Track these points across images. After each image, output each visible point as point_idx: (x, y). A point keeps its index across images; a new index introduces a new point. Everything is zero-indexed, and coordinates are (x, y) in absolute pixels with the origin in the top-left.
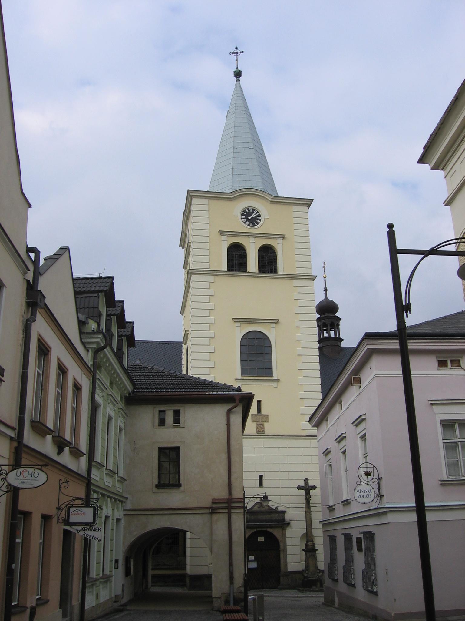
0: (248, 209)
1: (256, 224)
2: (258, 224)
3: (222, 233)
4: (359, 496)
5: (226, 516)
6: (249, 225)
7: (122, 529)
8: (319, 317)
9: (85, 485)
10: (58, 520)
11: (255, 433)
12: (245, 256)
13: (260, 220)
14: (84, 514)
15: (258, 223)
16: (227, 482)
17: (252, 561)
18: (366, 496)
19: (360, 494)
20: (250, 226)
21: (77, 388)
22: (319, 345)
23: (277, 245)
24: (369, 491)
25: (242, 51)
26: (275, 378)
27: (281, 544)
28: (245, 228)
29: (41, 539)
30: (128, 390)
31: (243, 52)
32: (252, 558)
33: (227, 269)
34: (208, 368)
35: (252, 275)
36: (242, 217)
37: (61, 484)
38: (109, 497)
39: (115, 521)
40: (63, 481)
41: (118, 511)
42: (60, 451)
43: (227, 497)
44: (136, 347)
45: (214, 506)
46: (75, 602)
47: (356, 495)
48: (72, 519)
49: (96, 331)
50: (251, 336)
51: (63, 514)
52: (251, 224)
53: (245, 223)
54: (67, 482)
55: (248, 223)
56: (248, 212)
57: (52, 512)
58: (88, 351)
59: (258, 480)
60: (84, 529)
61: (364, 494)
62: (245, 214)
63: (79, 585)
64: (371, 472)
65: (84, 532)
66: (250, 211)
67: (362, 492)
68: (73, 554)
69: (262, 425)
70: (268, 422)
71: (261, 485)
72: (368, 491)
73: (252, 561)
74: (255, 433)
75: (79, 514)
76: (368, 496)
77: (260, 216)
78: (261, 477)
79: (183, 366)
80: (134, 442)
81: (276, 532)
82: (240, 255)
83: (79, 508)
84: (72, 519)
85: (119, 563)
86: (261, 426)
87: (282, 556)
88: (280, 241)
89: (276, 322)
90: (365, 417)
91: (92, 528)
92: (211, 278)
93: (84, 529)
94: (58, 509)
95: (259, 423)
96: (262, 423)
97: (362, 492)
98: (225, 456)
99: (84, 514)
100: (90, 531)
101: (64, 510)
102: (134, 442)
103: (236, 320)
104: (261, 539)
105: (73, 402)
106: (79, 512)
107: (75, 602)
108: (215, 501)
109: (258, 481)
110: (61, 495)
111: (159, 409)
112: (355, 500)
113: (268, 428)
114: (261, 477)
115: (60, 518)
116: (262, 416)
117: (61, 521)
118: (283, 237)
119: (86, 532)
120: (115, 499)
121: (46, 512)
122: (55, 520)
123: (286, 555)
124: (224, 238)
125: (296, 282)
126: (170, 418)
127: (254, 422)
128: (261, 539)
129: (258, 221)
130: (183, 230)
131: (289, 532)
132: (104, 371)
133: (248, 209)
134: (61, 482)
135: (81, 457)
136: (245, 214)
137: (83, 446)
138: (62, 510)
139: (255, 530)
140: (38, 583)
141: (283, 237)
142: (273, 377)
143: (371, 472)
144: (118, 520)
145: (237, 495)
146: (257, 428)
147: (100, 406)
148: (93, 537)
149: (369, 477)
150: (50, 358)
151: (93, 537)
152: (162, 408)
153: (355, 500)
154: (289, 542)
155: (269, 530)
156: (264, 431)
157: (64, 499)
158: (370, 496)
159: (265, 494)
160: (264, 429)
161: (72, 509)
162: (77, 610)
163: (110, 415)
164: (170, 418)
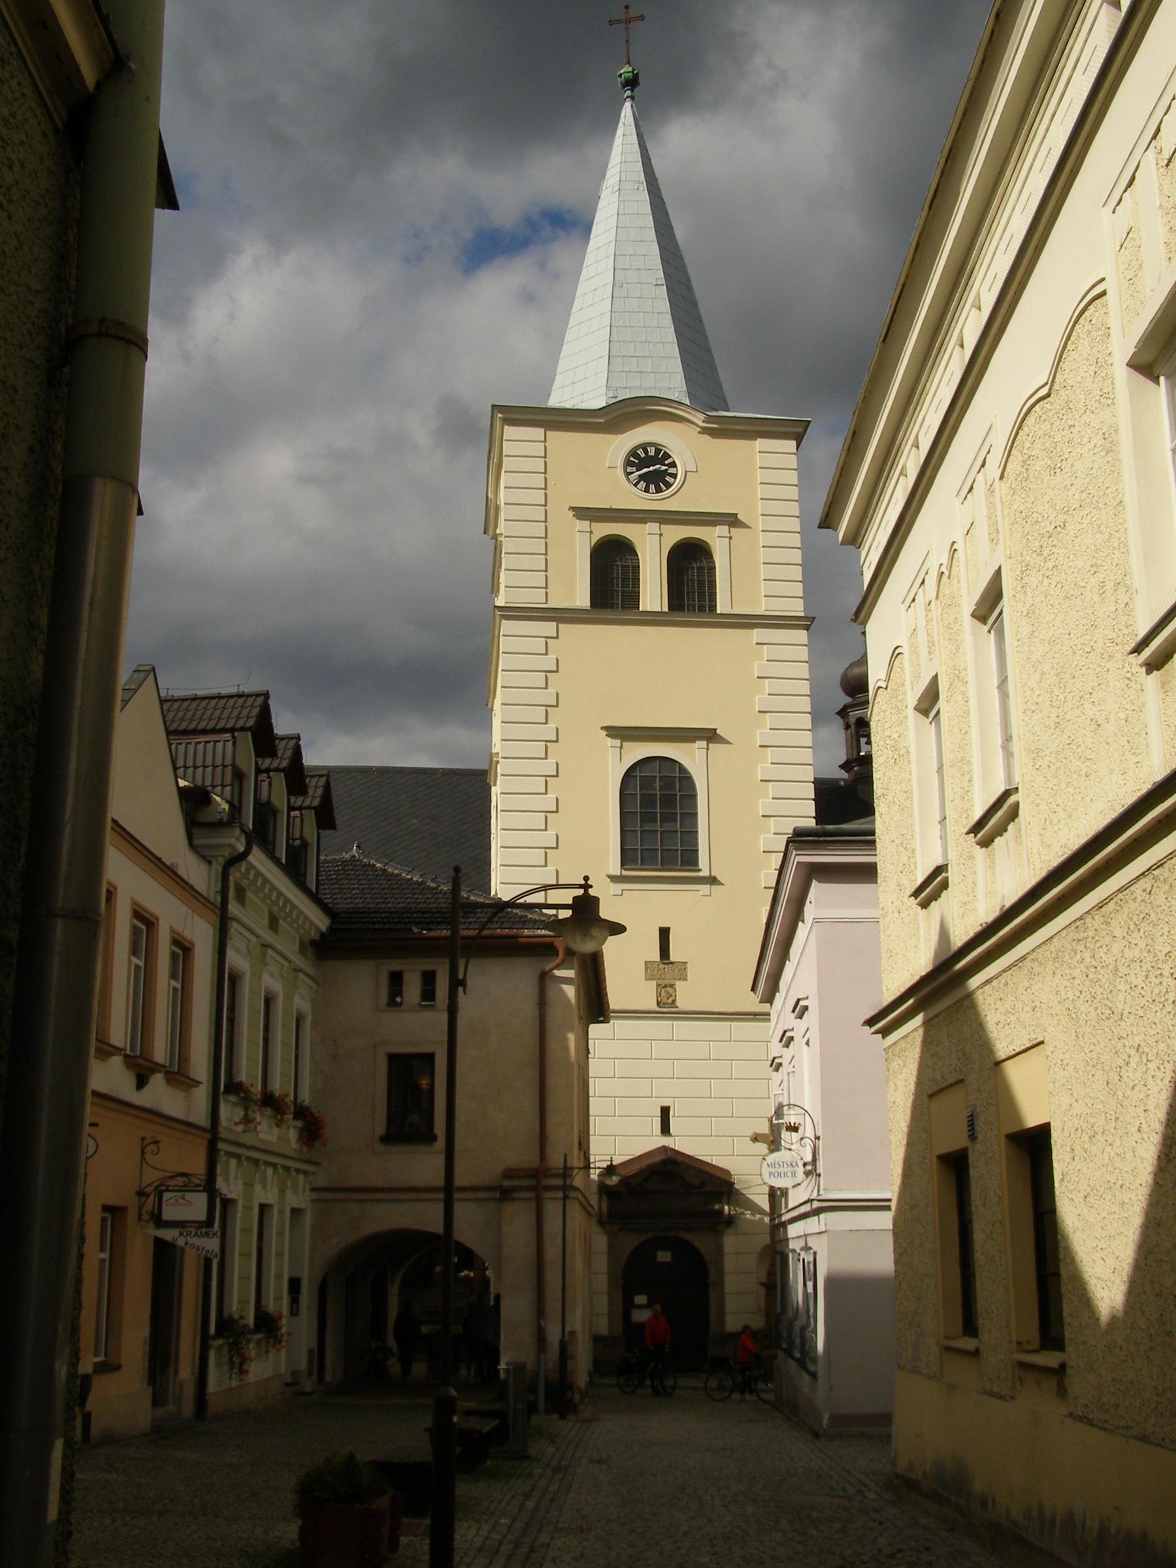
0: (646, 452)
1: (664, 488)
2: (675, 478)
3: (582, 513)
4: (771, 1174)
5: (533, 1205)
6: (647, 490)
7: (308, 1232)
8: (848, 701)
9: (205, 1143)
10: (140, 1215)
11: (653, 1006)
12: (636, 569)
13: (674, 476)
14: (190, 1204)
15: (668, 485)
16: (538, 1132)
17: (641, 1307)
18: (785, 1174)
19: (773, 1170)
20: (648, 492)
21: (183, 949)
22: (847, 774)
23: (715, 537)
24: (794, 1164)
25: (642, 16)
26: (705, 873)
27: (712, 1270)
28: (635, 498)
29: (102, 1249)
30: (317, 929)
31: (642, 18)
32: (641, 1299)
33: (589, 604)
34: (540, 850)
35: (652, 619)
36: (629, 469)
37: (147, 1146)
38: (267, 1164)
39: (288, 1214)
40: (149, 1140)
41: (295, 1192)
42: (141, 1082)
43: (536, 1163)
44: (338, 828)
45: (506, 1183)
46: (186, 1371)
47: (766, 1171)
48: (168, 1214)
49: (225, 820)
50: (654, 771)
51: (150, 1203)
52: (652, 487)
53: (636, 485)
54: (156, 1142)
55: (642, 484)
56: (643, 455)
57: (131, 1202)
58: (210, 863)
59: (660, 1118)
60: (185, 1234)
61: (781, 1170)
62: (636, 461)
63: (195, 1343)
64: (799, 1124)
65: (185, 1239)
66: (650, 454)
67: (777, 1166)
68: (181, 1280)
69: (672, 986)
70: (685, 979)
71: (665, 1129)
72: (791, 1165)
73: (641, 1307)
74: (653, 1006)
75: (180, 1205)
76: (789, 1174)
77: (676, 466)
78: (665, 1112)
79: (492, 836)
80: (334, 1041)
81: (701, 1242)
82: (622, 566)
83: (180, 1194)
84: (168, 1214)
85: (301, 1302)
86: (670, 990)
87: (713, 1295)
88: (722, 530)
89: (711, 736)
90: (807, 1004)
91: (201, 1232)
92: (549, 628)
93: (185, 1234)
94: (141, 1194)
95: (663, 982)
96: (672, 982)
97: (777, 1166)
98: (532, 1074)
99: (190, 1204)
100: (196, 1238)
101: (152, 1196)
102: (334, 1041)
103: (613, 732)
104: (664, 1256)
105: (173, 976)
106: (181, 1201)
107: (186, 1371)
108: (509, 1174)
109: (657, 1122)
110: (145, 1165)
111: (390, 969)
112: (764, 1183)
113: (686, 996)
114: (665, 1112)
115: (144, 1211)
116: (670, 966)
117: (146, 1217)
118: (732, 520)
119: (191, 1240)
120: (287, 1169)
121: (114, 1201)
122: (132, 1215)
123: (722, 1295)
124: (585, 525)
125: (757, 634)
126: (412, 988)
127: (650, 979)
128: (664, 1256)
129: (668, 479)
130: (489, 496)
131: (730, 1242)
132: (253, 897)
133: (646, 452)
134: (146, 1142)
135: (194, 1090)
136: (636, 461)
137: (200, 1064)
138: (148, 1196)
139: (650, 1235)
140: (98, 1329)
141: (732, 520)
142: (700, 870)
143: (799, 1124)
144: (296, 1212)
145: (555, 1160)
146: (659, 995)
147: (244, 974)
148: (203, 1248)
149: (793, 1134)
150: (115, 900)
151: (203, 1248)
152: (395, 965)
153: (764, 1183)
154: (729, 1264)
155: (684, 1235)
156: (674, 1001)
157: (151, 1177)
158: (794, 1174)
159: (611, 1161)
160: (676, 996)
161: (166, 1196)
162: (189, 1392)
163: (1155, 383)
164: (412, 988)
